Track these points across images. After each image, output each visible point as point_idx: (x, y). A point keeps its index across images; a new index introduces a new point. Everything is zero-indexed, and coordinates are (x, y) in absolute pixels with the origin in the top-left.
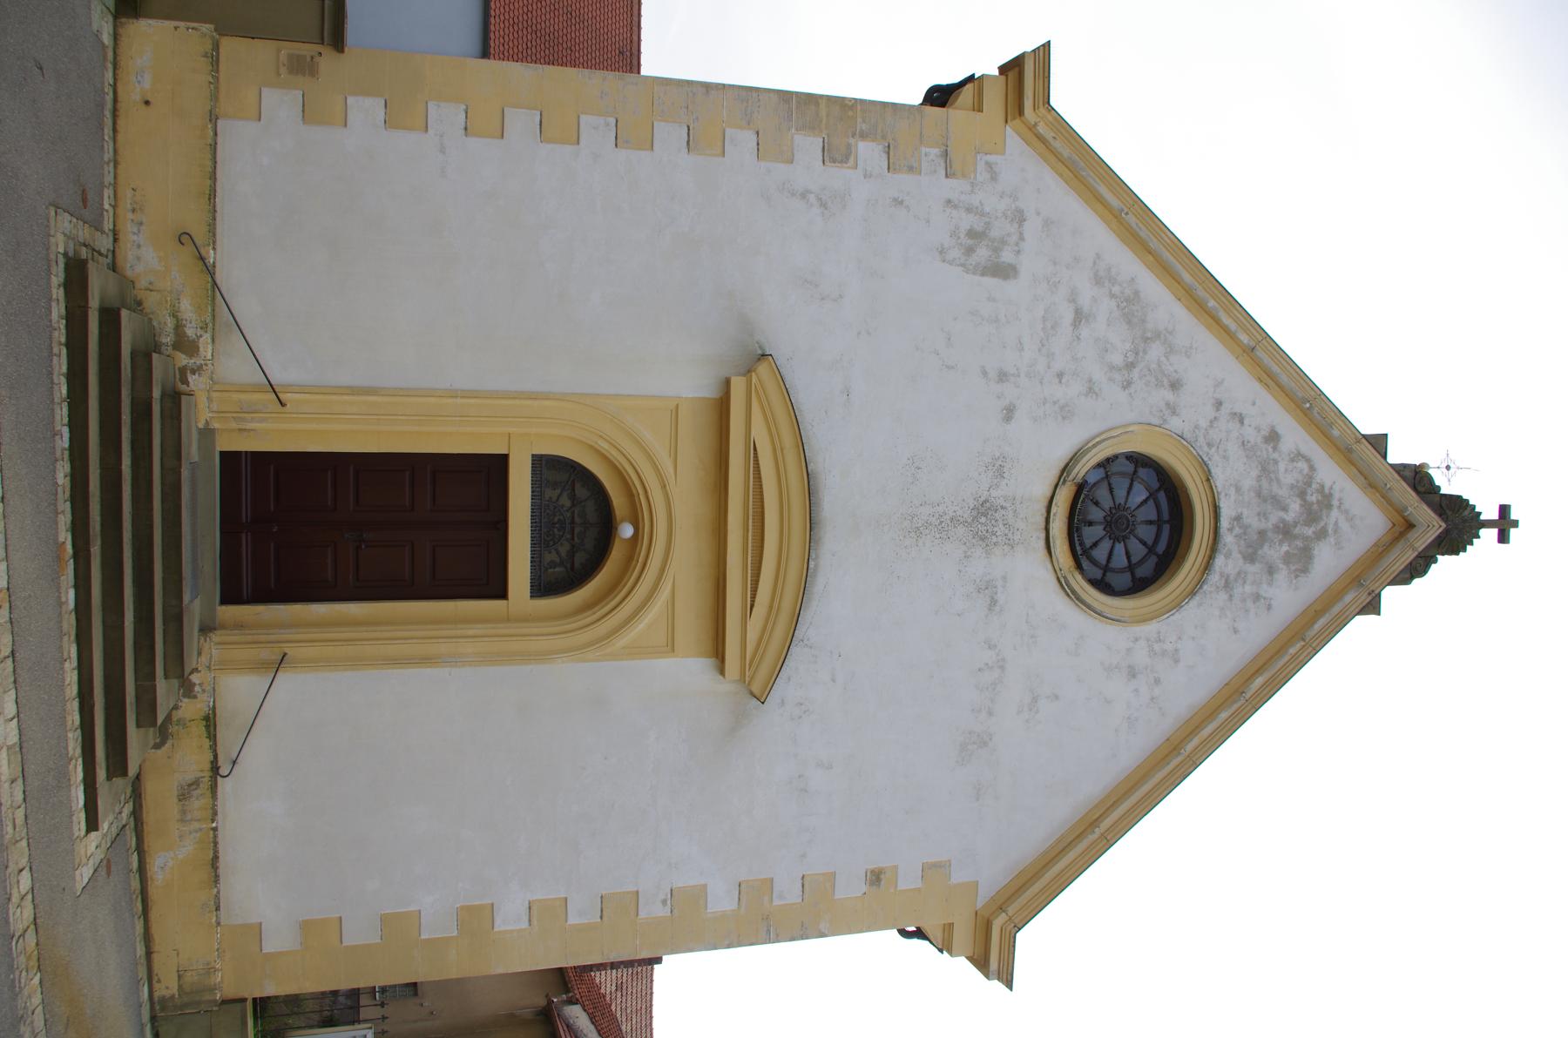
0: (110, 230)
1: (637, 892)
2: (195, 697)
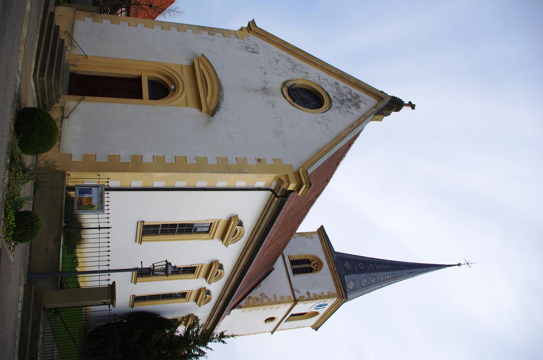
0: (21, 300)
1: (186, 157)
2: (59, 103)
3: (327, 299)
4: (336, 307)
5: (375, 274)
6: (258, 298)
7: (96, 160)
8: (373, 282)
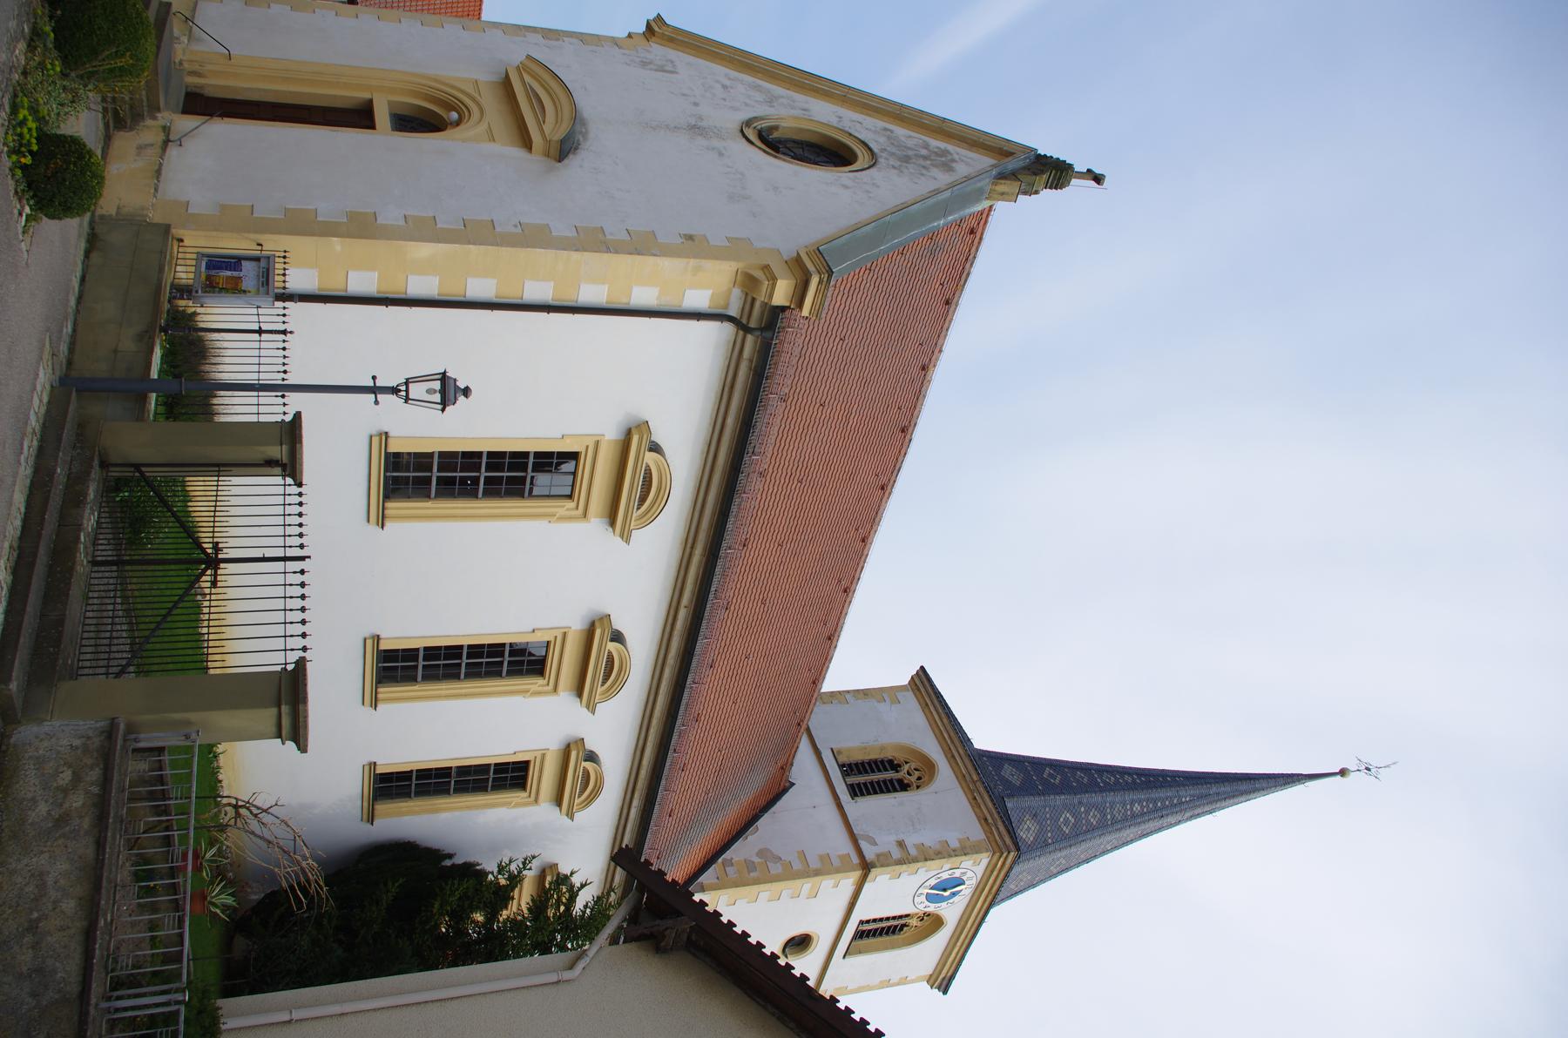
1: (492, 221)
3: (958, 859)
4: (991, 889)
5: (1096, 798)
6: (753, 862)
7: (252, 214)
8: (1094, 823)
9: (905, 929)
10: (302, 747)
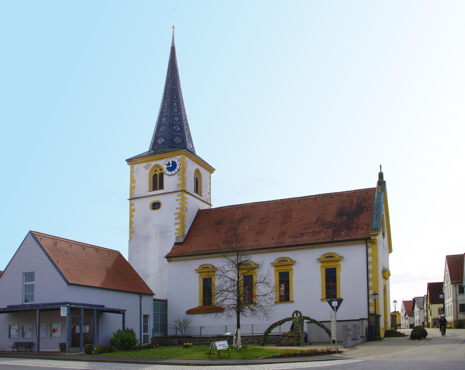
9: (197, 179)
10: (126, 310)
